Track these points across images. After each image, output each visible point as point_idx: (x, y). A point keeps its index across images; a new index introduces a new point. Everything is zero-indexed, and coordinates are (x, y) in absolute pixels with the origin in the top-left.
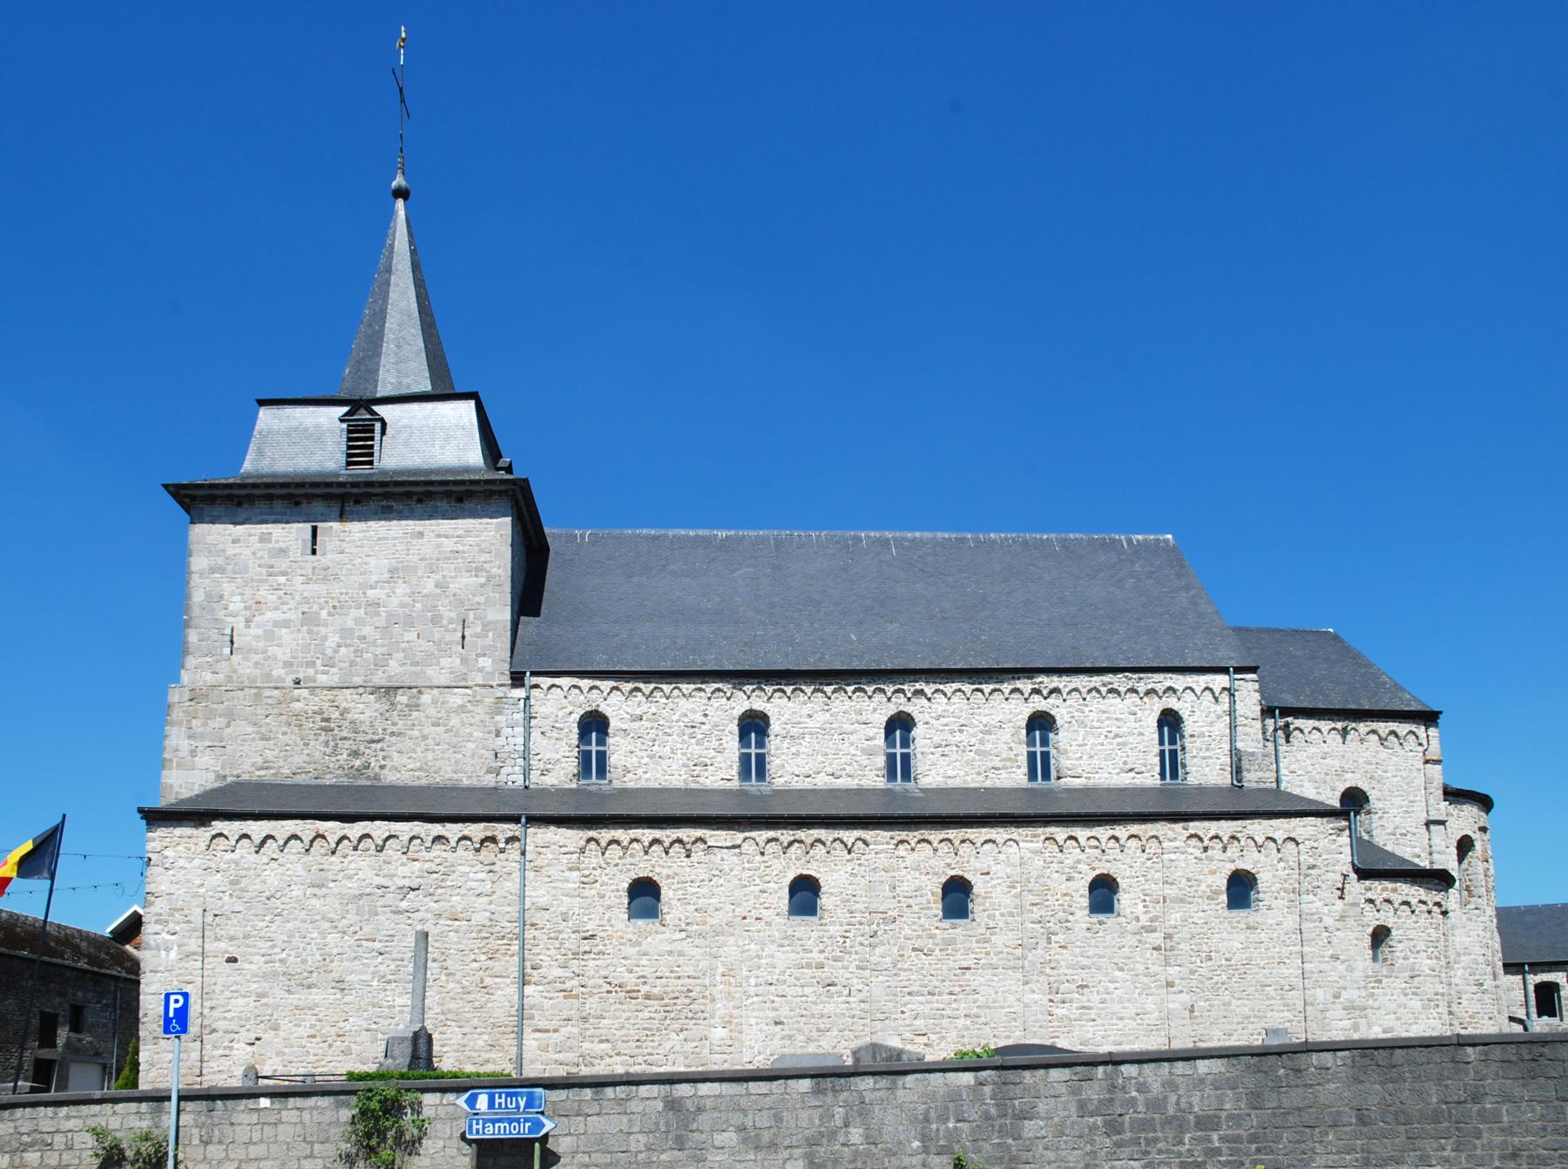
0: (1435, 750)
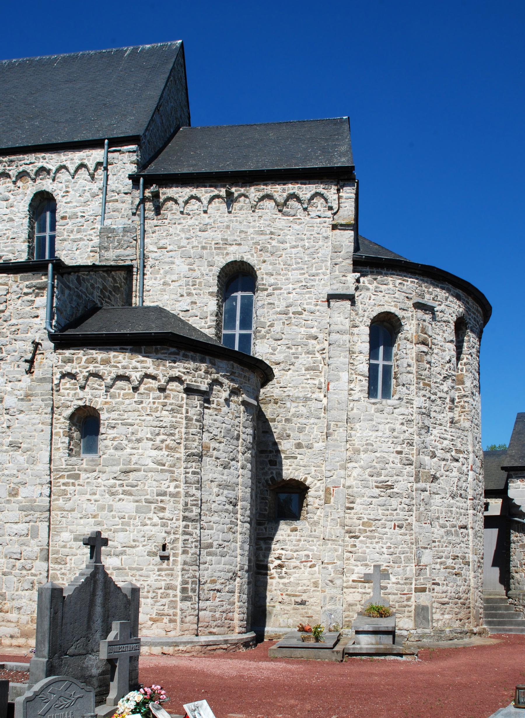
0: (347, 212)
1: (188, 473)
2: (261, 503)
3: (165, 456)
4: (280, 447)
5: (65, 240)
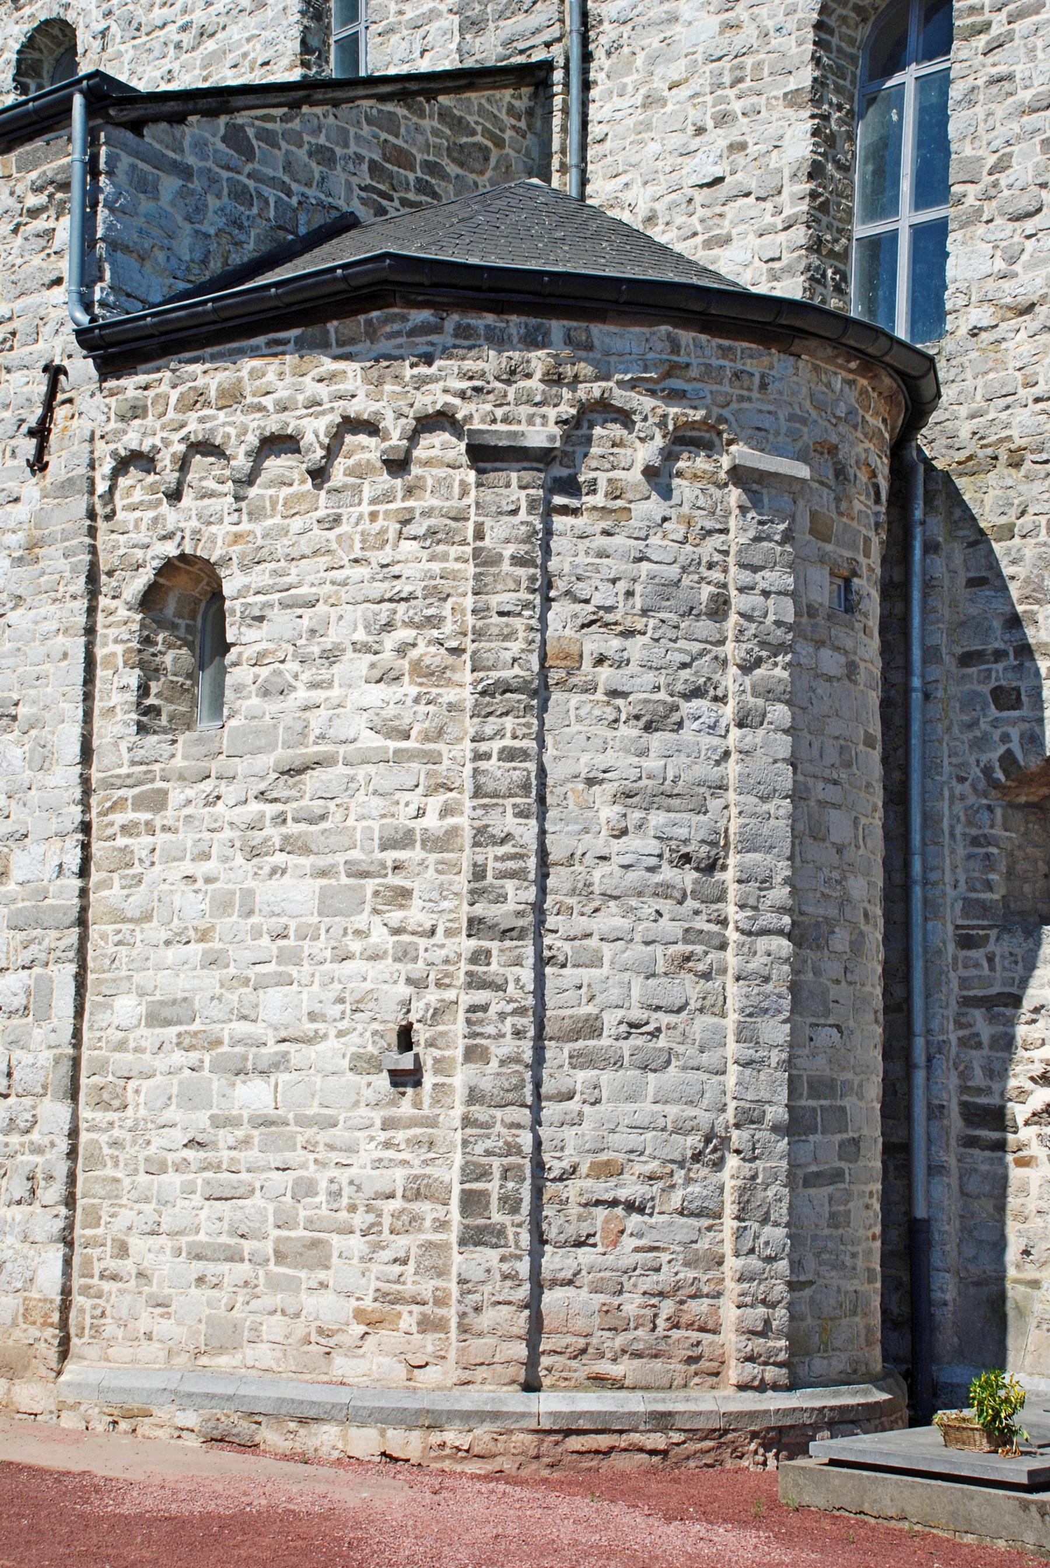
1: (487, 756)
2: (970, 857)
3: (409, 702)
4: (1030, 632)
5: (392, 30)
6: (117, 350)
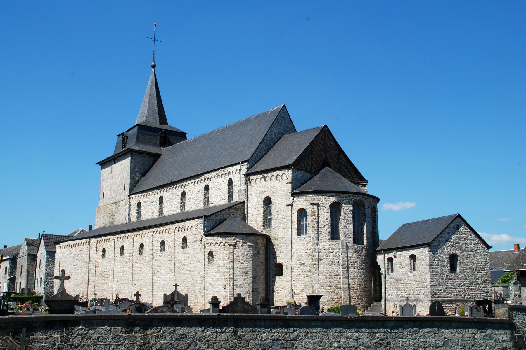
6: (206, 235)
